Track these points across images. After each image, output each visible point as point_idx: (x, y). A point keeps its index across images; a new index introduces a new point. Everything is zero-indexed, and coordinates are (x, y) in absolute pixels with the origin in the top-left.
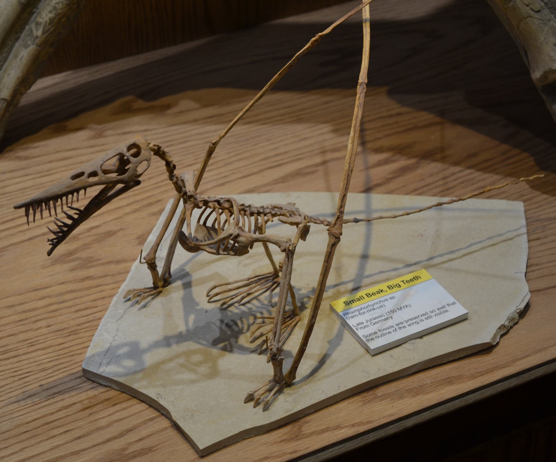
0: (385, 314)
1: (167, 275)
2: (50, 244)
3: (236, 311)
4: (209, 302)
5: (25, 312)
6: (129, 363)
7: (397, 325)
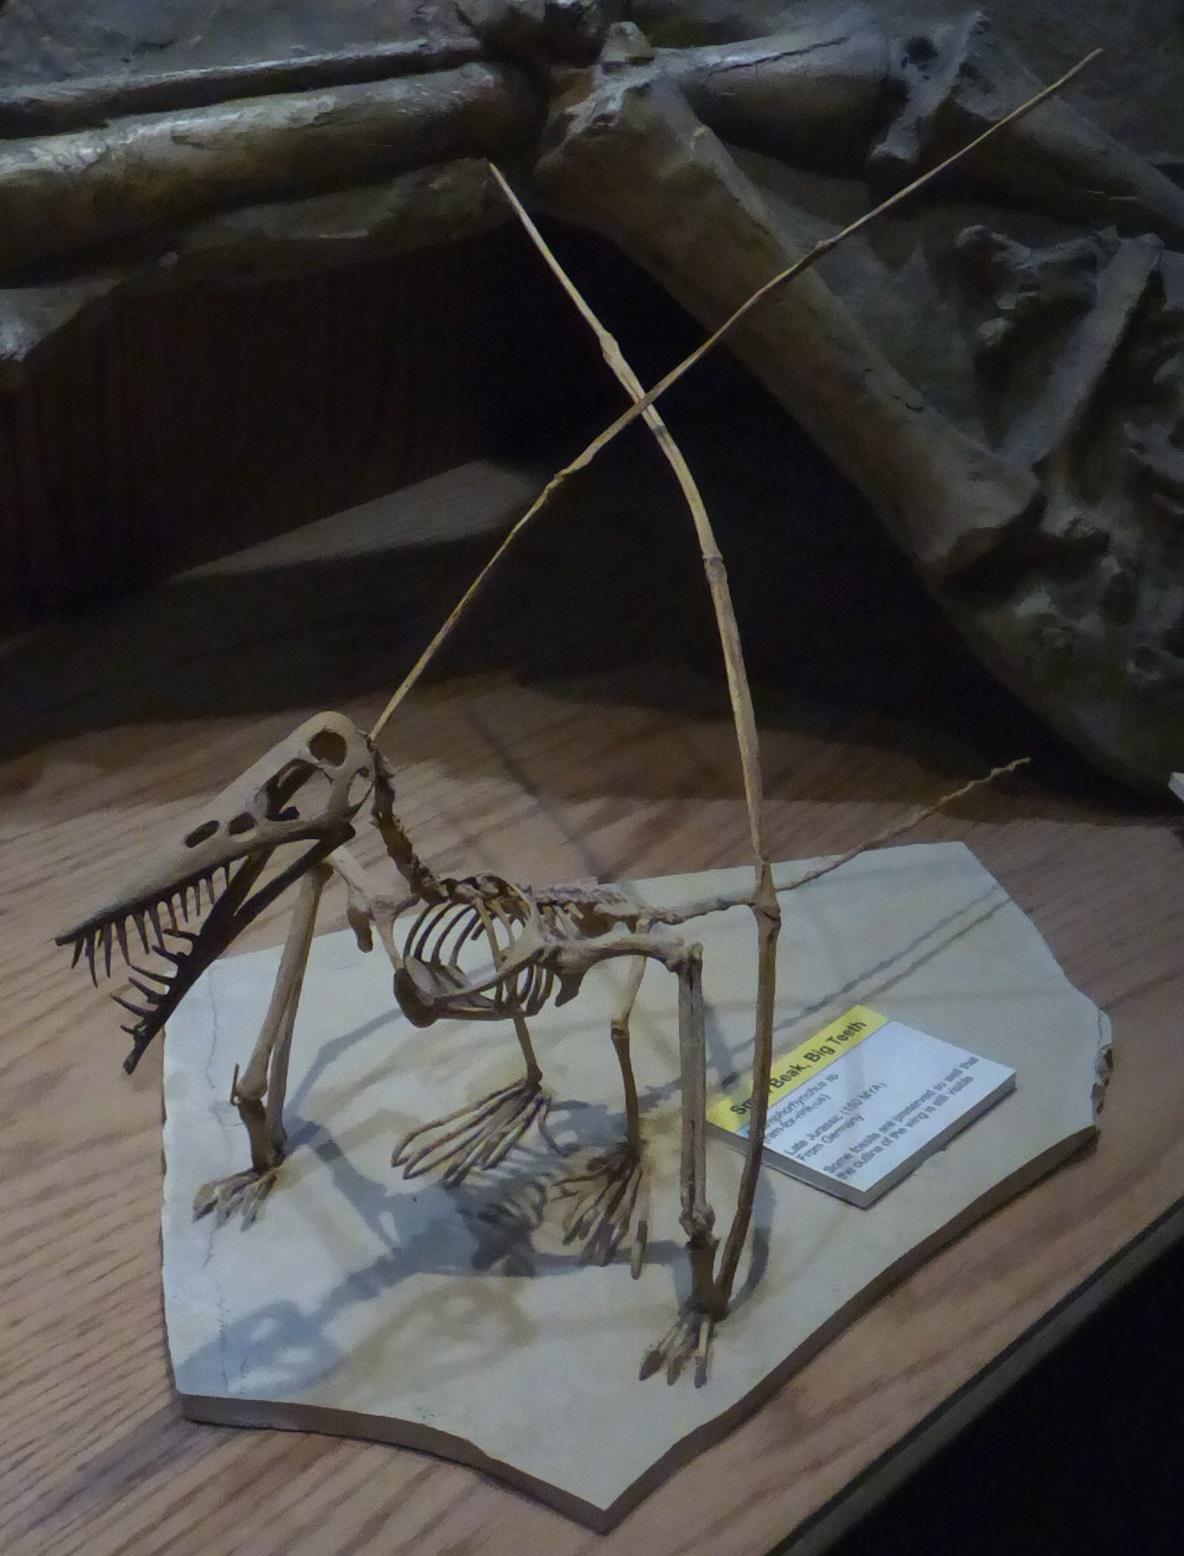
0: (841, 1114)
3: (484, 1183)
4: (406, 1177)
6: (297, 1356)
7: (884, 1129)
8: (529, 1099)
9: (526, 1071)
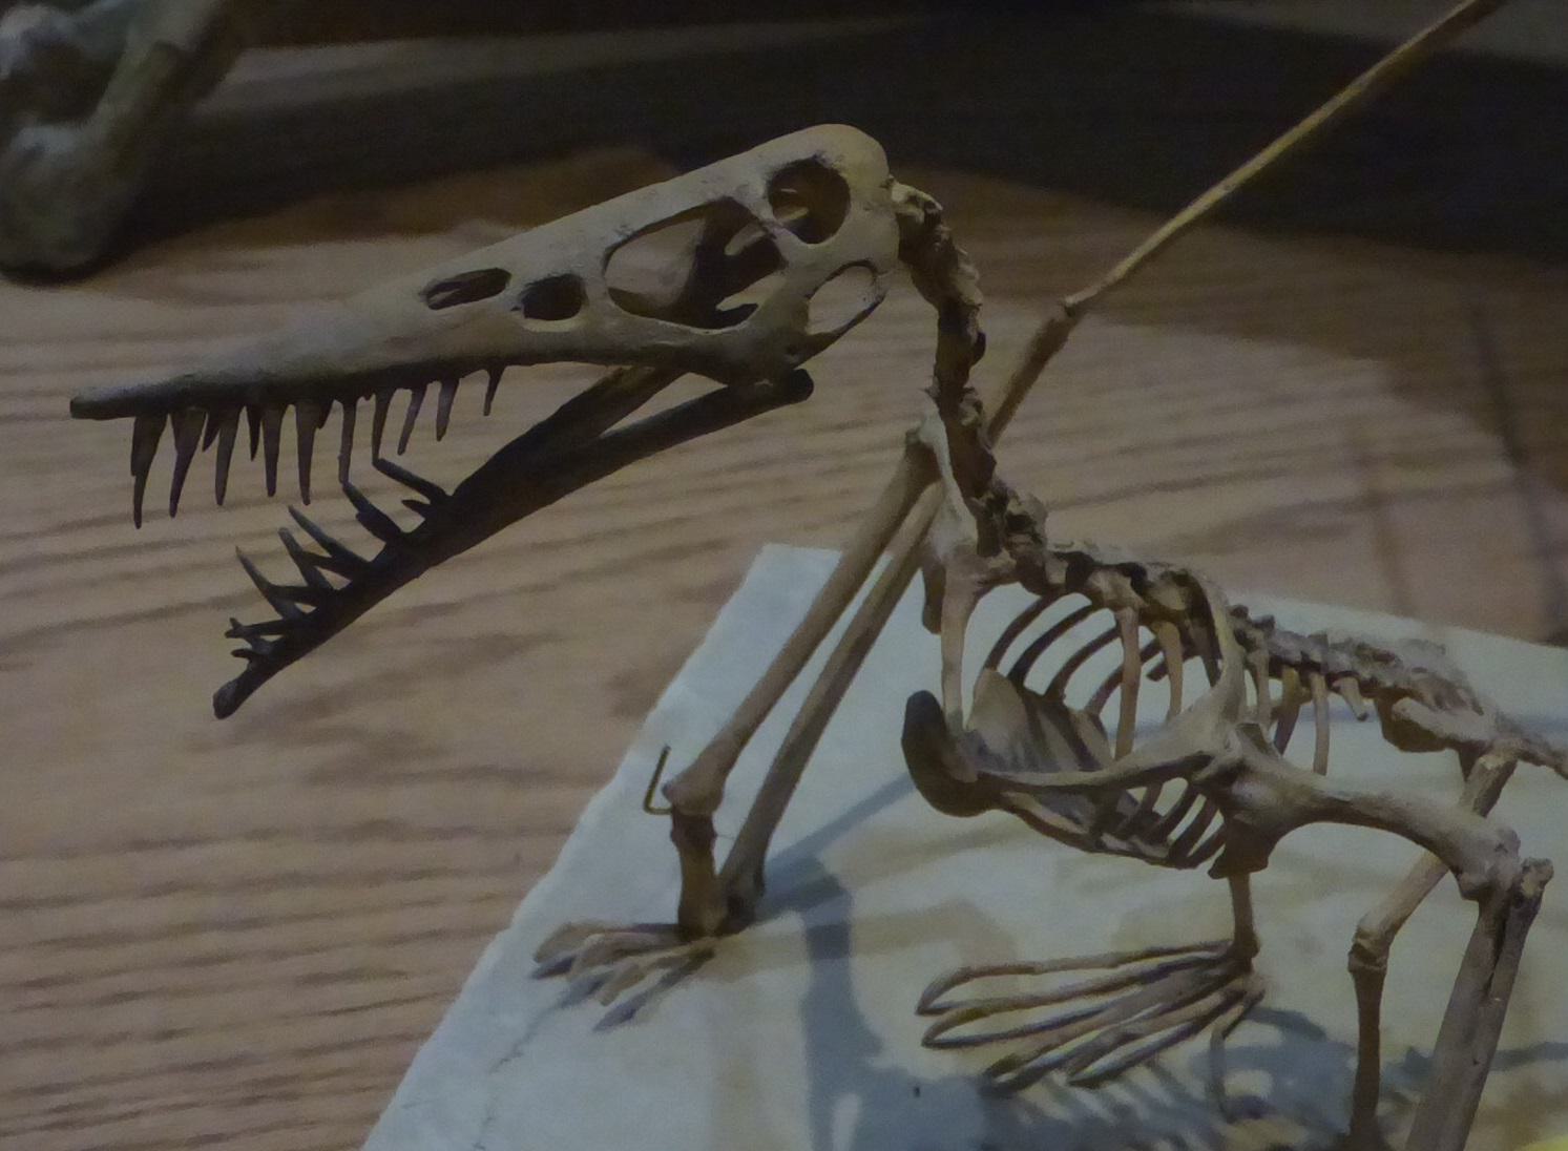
1: (747, 882)
2: (238, 653)
3: (1058, 1112)
5: (75, 942)
8: (1221, 982)
9: (1232, 928)
